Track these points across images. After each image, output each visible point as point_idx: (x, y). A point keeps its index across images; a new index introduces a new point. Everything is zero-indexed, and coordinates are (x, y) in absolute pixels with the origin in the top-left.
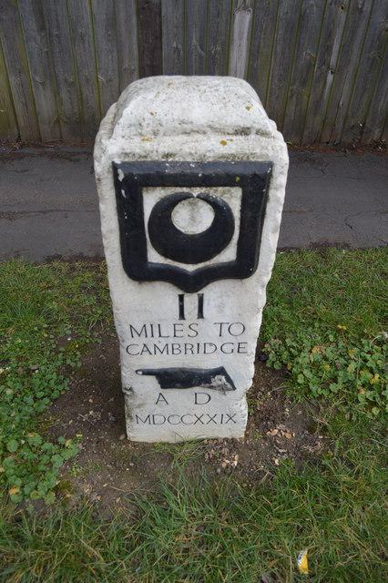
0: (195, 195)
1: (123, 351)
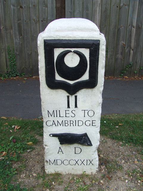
1: (44, 124)
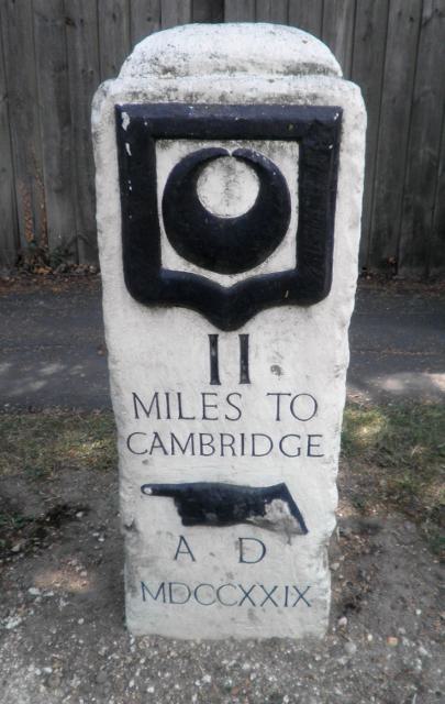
0: (230, 152)
1: (122, 447)
